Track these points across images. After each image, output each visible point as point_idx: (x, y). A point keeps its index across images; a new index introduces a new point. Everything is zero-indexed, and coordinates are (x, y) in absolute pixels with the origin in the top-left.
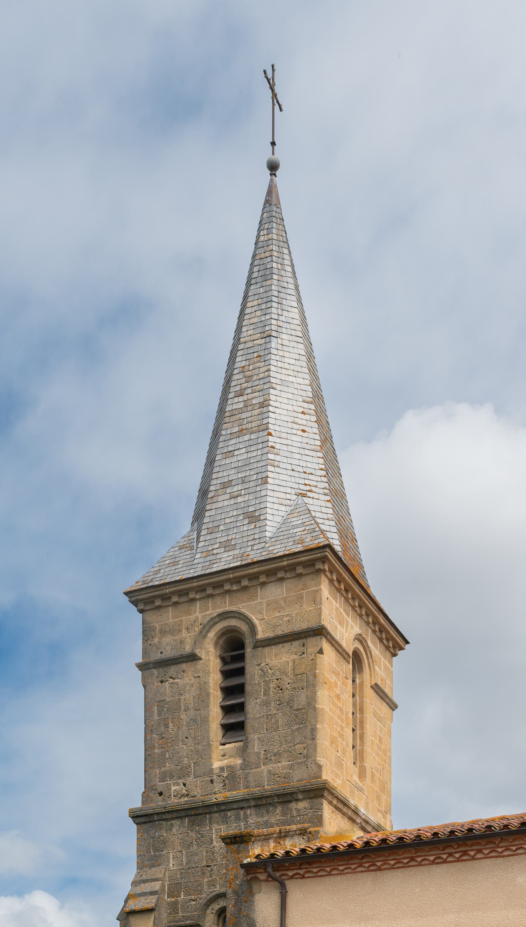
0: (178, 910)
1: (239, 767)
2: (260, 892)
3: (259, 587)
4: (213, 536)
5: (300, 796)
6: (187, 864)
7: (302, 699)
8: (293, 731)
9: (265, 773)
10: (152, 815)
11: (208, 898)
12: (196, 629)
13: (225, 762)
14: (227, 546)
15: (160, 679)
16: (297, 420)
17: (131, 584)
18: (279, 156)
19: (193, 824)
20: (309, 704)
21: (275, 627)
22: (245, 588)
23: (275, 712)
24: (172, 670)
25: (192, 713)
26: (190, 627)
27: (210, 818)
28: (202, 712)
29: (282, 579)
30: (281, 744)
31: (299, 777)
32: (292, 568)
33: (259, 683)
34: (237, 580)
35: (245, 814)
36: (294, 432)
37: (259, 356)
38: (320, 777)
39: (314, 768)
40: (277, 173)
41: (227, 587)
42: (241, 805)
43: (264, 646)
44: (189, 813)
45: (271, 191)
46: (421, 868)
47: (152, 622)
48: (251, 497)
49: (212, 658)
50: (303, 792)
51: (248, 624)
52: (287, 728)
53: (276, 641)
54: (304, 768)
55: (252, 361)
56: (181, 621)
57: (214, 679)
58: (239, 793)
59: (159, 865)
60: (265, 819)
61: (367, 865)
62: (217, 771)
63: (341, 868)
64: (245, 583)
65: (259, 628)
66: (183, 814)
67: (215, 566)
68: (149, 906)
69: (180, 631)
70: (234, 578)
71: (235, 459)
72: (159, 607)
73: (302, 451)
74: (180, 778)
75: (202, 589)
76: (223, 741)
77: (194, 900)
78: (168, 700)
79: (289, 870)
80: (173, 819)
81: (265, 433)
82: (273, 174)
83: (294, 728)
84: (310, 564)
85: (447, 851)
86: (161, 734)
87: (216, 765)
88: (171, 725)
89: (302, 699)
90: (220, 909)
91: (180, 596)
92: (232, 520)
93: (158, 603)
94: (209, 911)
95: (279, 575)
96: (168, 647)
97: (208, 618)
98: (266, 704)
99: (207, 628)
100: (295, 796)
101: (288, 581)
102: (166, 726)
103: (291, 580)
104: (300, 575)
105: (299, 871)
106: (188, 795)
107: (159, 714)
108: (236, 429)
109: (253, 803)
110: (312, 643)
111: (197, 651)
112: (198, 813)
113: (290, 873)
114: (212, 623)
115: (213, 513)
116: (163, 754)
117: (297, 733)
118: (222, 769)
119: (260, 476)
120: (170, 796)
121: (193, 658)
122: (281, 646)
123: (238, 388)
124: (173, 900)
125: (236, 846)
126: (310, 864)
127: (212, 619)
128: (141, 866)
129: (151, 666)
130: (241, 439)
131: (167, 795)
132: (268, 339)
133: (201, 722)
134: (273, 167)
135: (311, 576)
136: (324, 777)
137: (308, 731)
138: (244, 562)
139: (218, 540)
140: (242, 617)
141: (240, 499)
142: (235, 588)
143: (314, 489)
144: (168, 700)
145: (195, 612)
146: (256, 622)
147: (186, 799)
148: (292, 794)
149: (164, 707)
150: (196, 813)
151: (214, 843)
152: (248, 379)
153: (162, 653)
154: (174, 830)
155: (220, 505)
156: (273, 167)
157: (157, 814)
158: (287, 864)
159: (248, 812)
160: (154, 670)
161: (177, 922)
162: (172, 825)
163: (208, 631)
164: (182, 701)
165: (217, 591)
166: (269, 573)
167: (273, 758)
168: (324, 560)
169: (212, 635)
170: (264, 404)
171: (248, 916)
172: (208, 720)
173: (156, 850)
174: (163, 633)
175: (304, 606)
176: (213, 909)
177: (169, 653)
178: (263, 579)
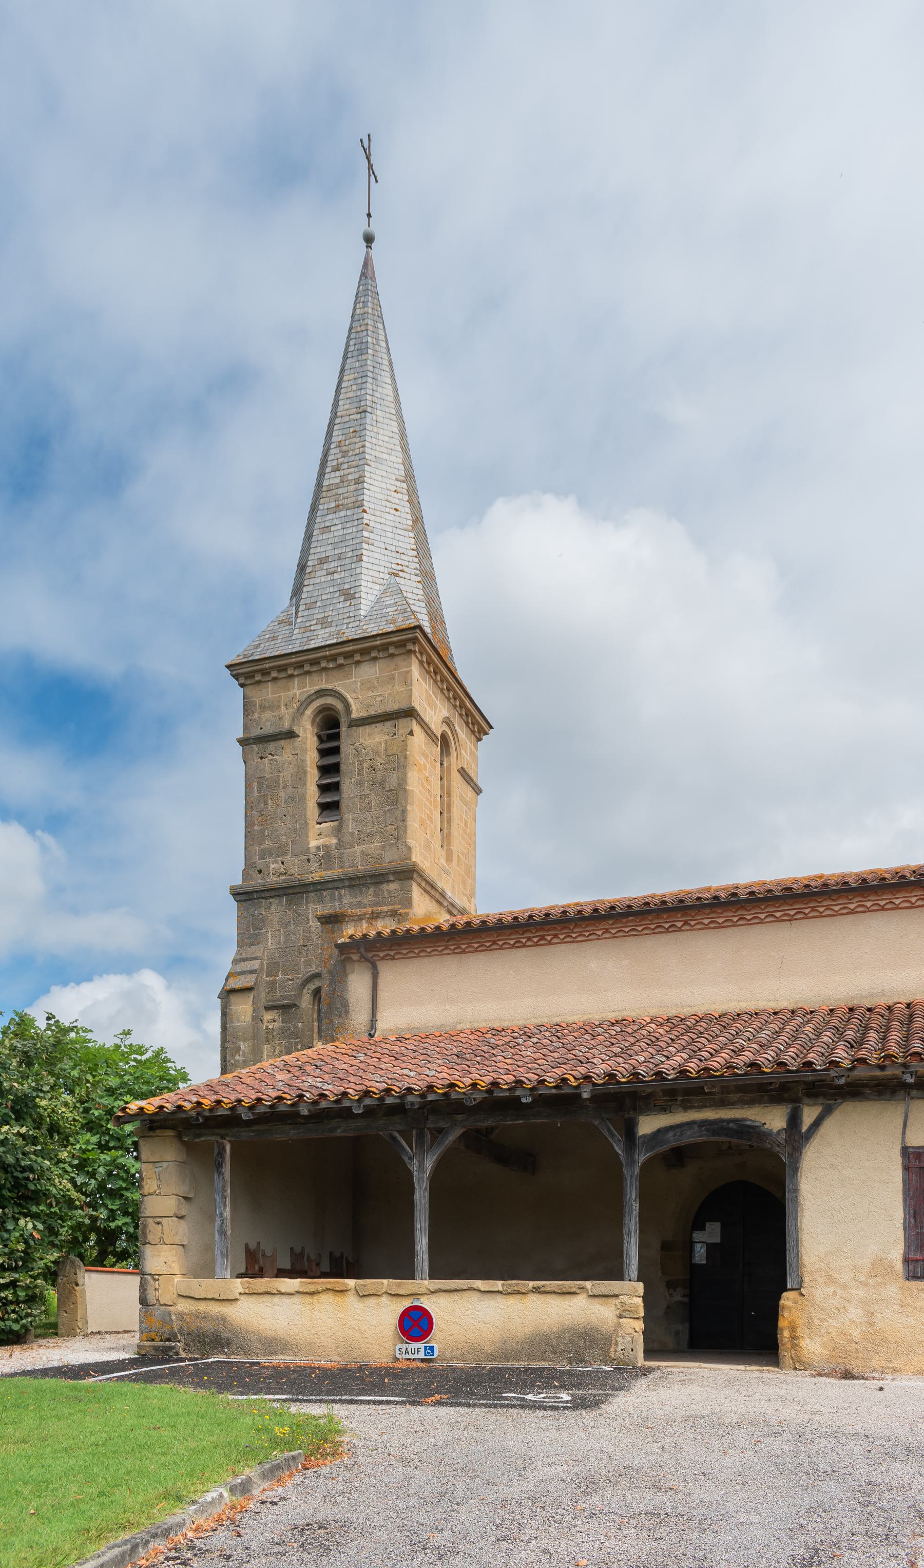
2: (353, 972)
4: (311, 612)
5: (391, 878)
8: (385, 812)
10: (252, 892)
13: (321, 842)
14: (324, 622)
15: (259, 755)
17: (232, 659)
18: (375, 229)
20: (400, 785)
21: (369, 706)
22: (341, 666)
24: (271, 746)
27: (307, 897)
29: (375, 659)
31: (390, 858)
32: (384, 648)
33: (354, 763)
34: (333, 658)
35: (340, 894)
36: (388, 510)
40: (373, 245)
42: (336, 885)
43: (358, 726)
45: (367, 263)
46: (502, 951)
53: (370, 720)
55: (348, 436)
57: (312, 758)
60: (358, 899)
61: (452, 948)
65: (354, 708)
66: (281, 892)
68: (249, 985)
69: (279, 707)
70: (331, 655)
72: (259, 682)
73: (395, 530)
74: (278, 856)
80: (272, 897)
81: (360, 510)
84: (401, 644)
87: (313, 844)
88: (270, 802)
93: (258, 677)
94: (305, 991)
95: (373, 655)
96: (267, 723)
97: (306, 695)
98: (360, 784)
99: (304, 705)
101: (381, 661)
102: (266, 803)
103: (384, 660)
104: (392, 656)
107: (259, 791)
108: (333, 505)
109: (347, 883)
110: (402, 722)
111: (295, 729)
113: (382, 954)
114: (309, 700)
115: (310, 588)
116: (262, 831)
118: (318, 848)
121: (291, 735)
122: (374, 726)
123: (335, 463)
125: (331, 926)
126: (399, 945)
130: (337, 515)
131: (266, 873)
134: (369, 239)
136: (414, 859)
137: (399, 812)
139: (315, 617)
141: (336, 576)
143: (405, 569)
145: (294, 688)
146: (351, 701)
148: (383, 875)
149: (263, 783)
152: (345, 454)
154: (273, 909)
155: (318, 580)
156: (369, 239)
157: (257, 892)
159: (343, 892)
160: (254, 746)
162: (271, 903)
163: (306, 709)
168: (415, 641)
169: (309, 712)
170: (359, 481)
174: (263, 708)
175: (396, 687)
177: (268, 729)
178: (357, 657)
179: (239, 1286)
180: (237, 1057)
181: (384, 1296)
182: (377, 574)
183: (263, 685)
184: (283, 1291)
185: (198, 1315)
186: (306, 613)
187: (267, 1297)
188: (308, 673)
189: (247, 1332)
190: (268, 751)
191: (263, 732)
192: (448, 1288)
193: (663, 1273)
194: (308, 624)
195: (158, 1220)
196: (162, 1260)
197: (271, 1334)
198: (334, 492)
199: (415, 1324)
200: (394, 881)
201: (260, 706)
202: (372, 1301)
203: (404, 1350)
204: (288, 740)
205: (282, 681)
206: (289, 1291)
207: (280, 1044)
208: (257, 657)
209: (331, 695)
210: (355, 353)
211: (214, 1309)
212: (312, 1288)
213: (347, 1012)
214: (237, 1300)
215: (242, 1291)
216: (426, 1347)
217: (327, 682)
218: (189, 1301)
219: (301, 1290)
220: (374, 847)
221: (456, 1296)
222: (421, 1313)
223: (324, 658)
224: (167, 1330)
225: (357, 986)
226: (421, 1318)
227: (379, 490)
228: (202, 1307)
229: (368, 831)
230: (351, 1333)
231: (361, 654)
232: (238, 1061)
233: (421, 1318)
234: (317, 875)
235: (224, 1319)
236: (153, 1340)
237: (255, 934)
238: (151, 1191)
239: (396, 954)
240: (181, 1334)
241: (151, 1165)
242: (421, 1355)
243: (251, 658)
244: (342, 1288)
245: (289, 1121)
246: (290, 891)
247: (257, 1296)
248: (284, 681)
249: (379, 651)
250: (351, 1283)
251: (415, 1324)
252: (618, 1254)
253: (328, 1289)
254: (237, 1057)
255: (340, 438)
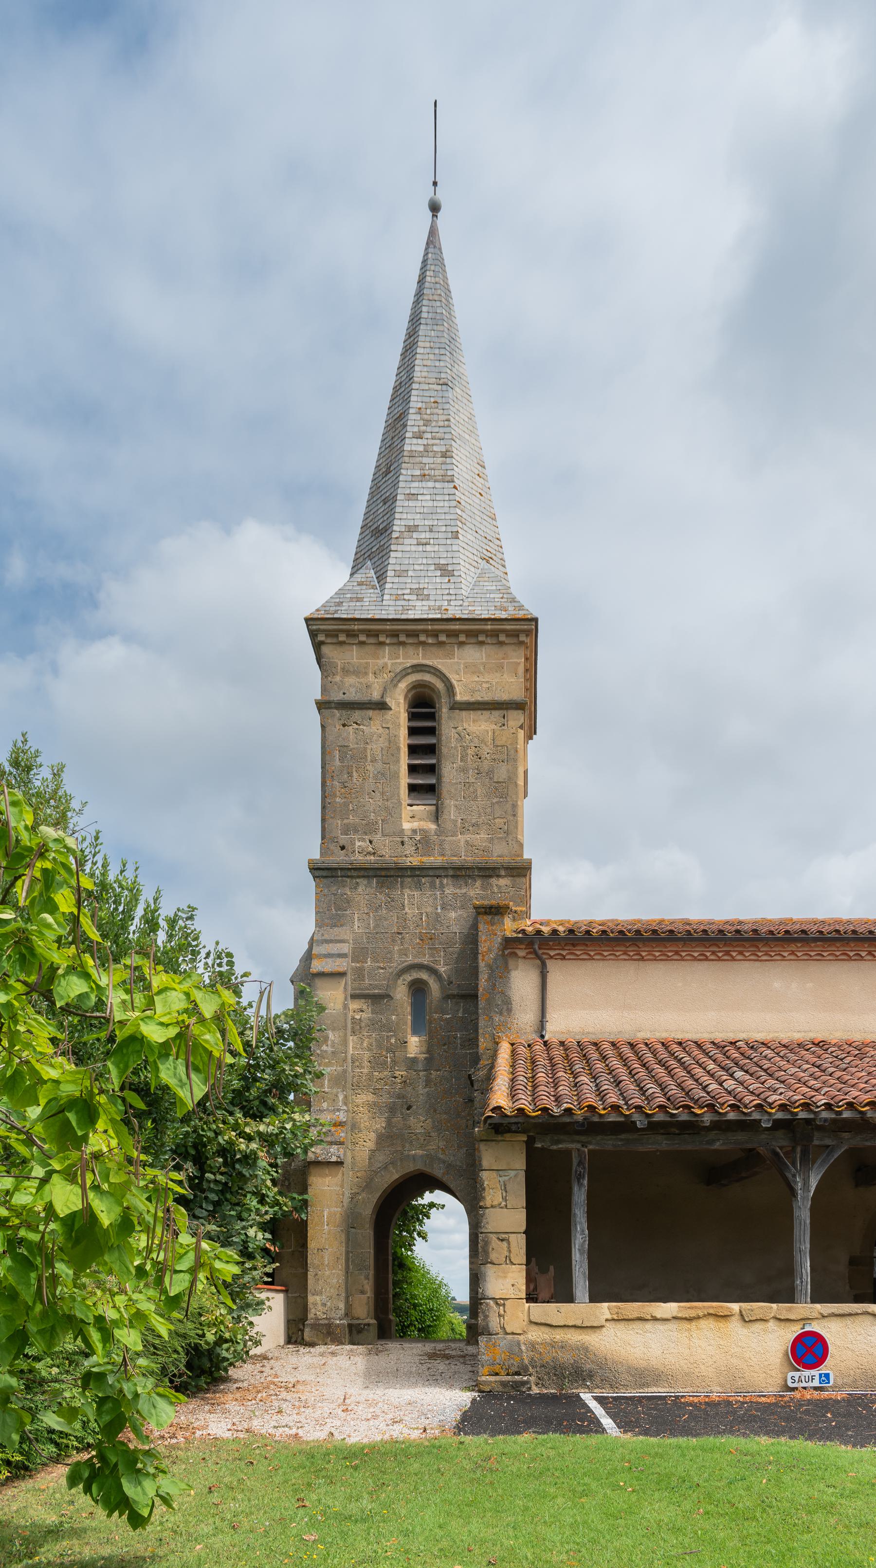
0: (364, 977)
1: (433, 832)
2: (517, 968)
3: (456, 646)
4: (402, 580)
6: (374, 928)
7: (502, 773)
8: (493, 804)
9: (462, 843)
10: (336, 869)
11: (400, 967)
12: (385, 675)
13: (415, 825)
14: (419, 593)
15: (342, 722)
16: (475, 481)
18: (442, 196)
19: (382, 886)
20: (510, 778)
21: (473, 691)
22: (441, 644)
23: (473, 781)
24: (357, 715)
25: (379, 765)
26: (378, 672)
27: (402, 882)
28: (392, 767)
29: (482, 643)
30: (480, 816)
31: (499, 853)
32: (495, 634)
33: (456, 748)
34: (435, 634)
35: (441, 883)
36: (474, 492)
37: (435, 402)
38: (522, 856)
39: (515, 846)
40: (439, 215)
41: (422, 638)
42: (438, 873)
43: (461, 709)
44: (378, 873)
45: (433, 232)
46: (683, 963)
47: (333, 658)
48: (442, 548)
49: (402, 711)
50: (507, 868)
51: (443, 681)
52: (486, 799)
53: (476, 706)
54: (504, 843)
55: (429, 405)
56: (366, 663)
58: (434, 860)
59: (342, 926)
60: (464, 891)
61: (631, 954)
62: (409, 833)
63: (605, 953)
64: (442, 638)
65: (458, 689)
66: (371, 873)
67: (410, 612)
68: (341, 970)
69: (366, 674)
70: (432, 631)
71: (419, 504)
72: (342, 643)
73: (481, 515)
74: (366, 834)
75: (395, 634)
76: (410, 802)
77: (382, 968)
78: (352, 746)
79: (551, 949)
80: (359, 877)
81: (451, 485)
82: (435, 216)
83: (494, 801)
85: (712, 949)
86: (343, 783)
87: (407, 826)
88: (355, 774)
89: (502, 773)
90: (412, 981)
91: (368, 636)
92: (422, 567)
93: (342, 638)
94: (400, 982)
96: (351, 688)
97: (400, 668)
98: (464, 770)
99: (398, 678)
100: (497, 871)
101: (487, 646)
102: (350, 774)
103: (491, 647)
104: (501, 643)
105: (562, 952)
106: (374, 853)
107: (341, 760)
108: (418, 473)
109: (451, 873)
111: (388, 700)
112: (389, 874)
113: (552, 953)
114: (404, 673)
115: (399, 555)
116: (346, 805)
117: (496, 806)
118: (414, 831)
119: (449, 529)
120: (354, 851)
121: (382, 706)
122: (479, 712)
123: (416, 429)
124: (358, 965)
125: (490, 917)
126: (574, 945)
127: (405, 669)
128: (319, 924)
129: (333, 705)
130: (424, 484)
131: (351, 850)
132: (444, 387)
133: (388, 776)
134: (435, 208)
135: (513, 647)
136: (525, 857)
137: (508, 807)
138: (445, 617)
139: (408, 586)
140: (438, 673)
141: (428, 548)
142: (430, 641)
143: (494, 557)
144: (352, 746)
145: (384, 657)
146: (455, 683)
147: (372, 858)
148: (494, 869)
149: (346, 753)
150: (387, 875)
151: (406, 909)
152: (427, 423)
153: (344, 694)
154: (360, 890)
155: (408, 548)
156: (435, 208)
157: (342, 869)
158: (551, 943)
159: (445, 881)
160: (336, 711)
161: (362, 989)
162: (357, 883)
163: (399, 681)
164: (369, 751)
165: (410, 641)
166: (470, 634)
167: (471, 828)
169: (403, 685)
171: (503, 993)
172: (398, 777)
173: (338, 908)
174: (346, 672)
175: (505, 676)
176: (404, 980)
177: (352, 695)
178: (462, 638)
179: (607, 1312)
180: (324, 1048)
181: (771, 1321)
182: (471, 556)
183: (346, 647)
184: (659, 1316)
185: (553, 1344)
186: (396, 580)
187: (638, 1325)
188: (403, 644)
189: (614, 1362)
190: (353, 719)
191: (346, 698)
192: (841, 1312)
193: (851, 1287)
194: (400, 592)
195: (504, 1236)
196: (509, 1281)
197: (643, 1364)
198: (418, 460)
199: (809, 1350)
200: (505, 876)
201: (343, 669)
202: (758, 1326)
203: (797, 1379)
204: (377, 712)
205: (370, 646)
206: (665, 1316)
207: (369, 1037)
208: (345, 616)
209: (429, 672)
210: (429, 321)
211: (574, 1337)
212: (692, 1313)
213: (509, 1010)
214: (602, 1327)
215: (609, 1317)
216: (820, 1375)
217: (424, 657)
218: (543, 1328)
219: (680, 1315)
220: (481, 838)
221: (848, 1321)
222: (815, 1339)
223: (425, 631)
224: (516, 1362)
225: (522, 982)
226: (814, 1345)
227: (465, 469)
228: (559, 1336)
229: (474, 821)
230: (735, 1361)
231: (467, 636)
232: (326, 1051)
233: (814, 1345)
234: (415, 861)
235: (586, 1349)
236: (497, 1374)
237: (337, 915)
238: (495, 1203)
239: (568, 954)
240: (533, 1367)
241: (494, 1174)
242: (816, 1383)
243: (336, 616)
244: (726, 1313)
245: (662, 1131)
246: (383, 873)
247: (626, 1323)
248: (373, 647)
249: (487, 636)
250: (735, 1307)
251: (809, 1350)
252: (789, 1271)
253: (710, 1314)
254: (324, 1048)
255: (420, 405)
